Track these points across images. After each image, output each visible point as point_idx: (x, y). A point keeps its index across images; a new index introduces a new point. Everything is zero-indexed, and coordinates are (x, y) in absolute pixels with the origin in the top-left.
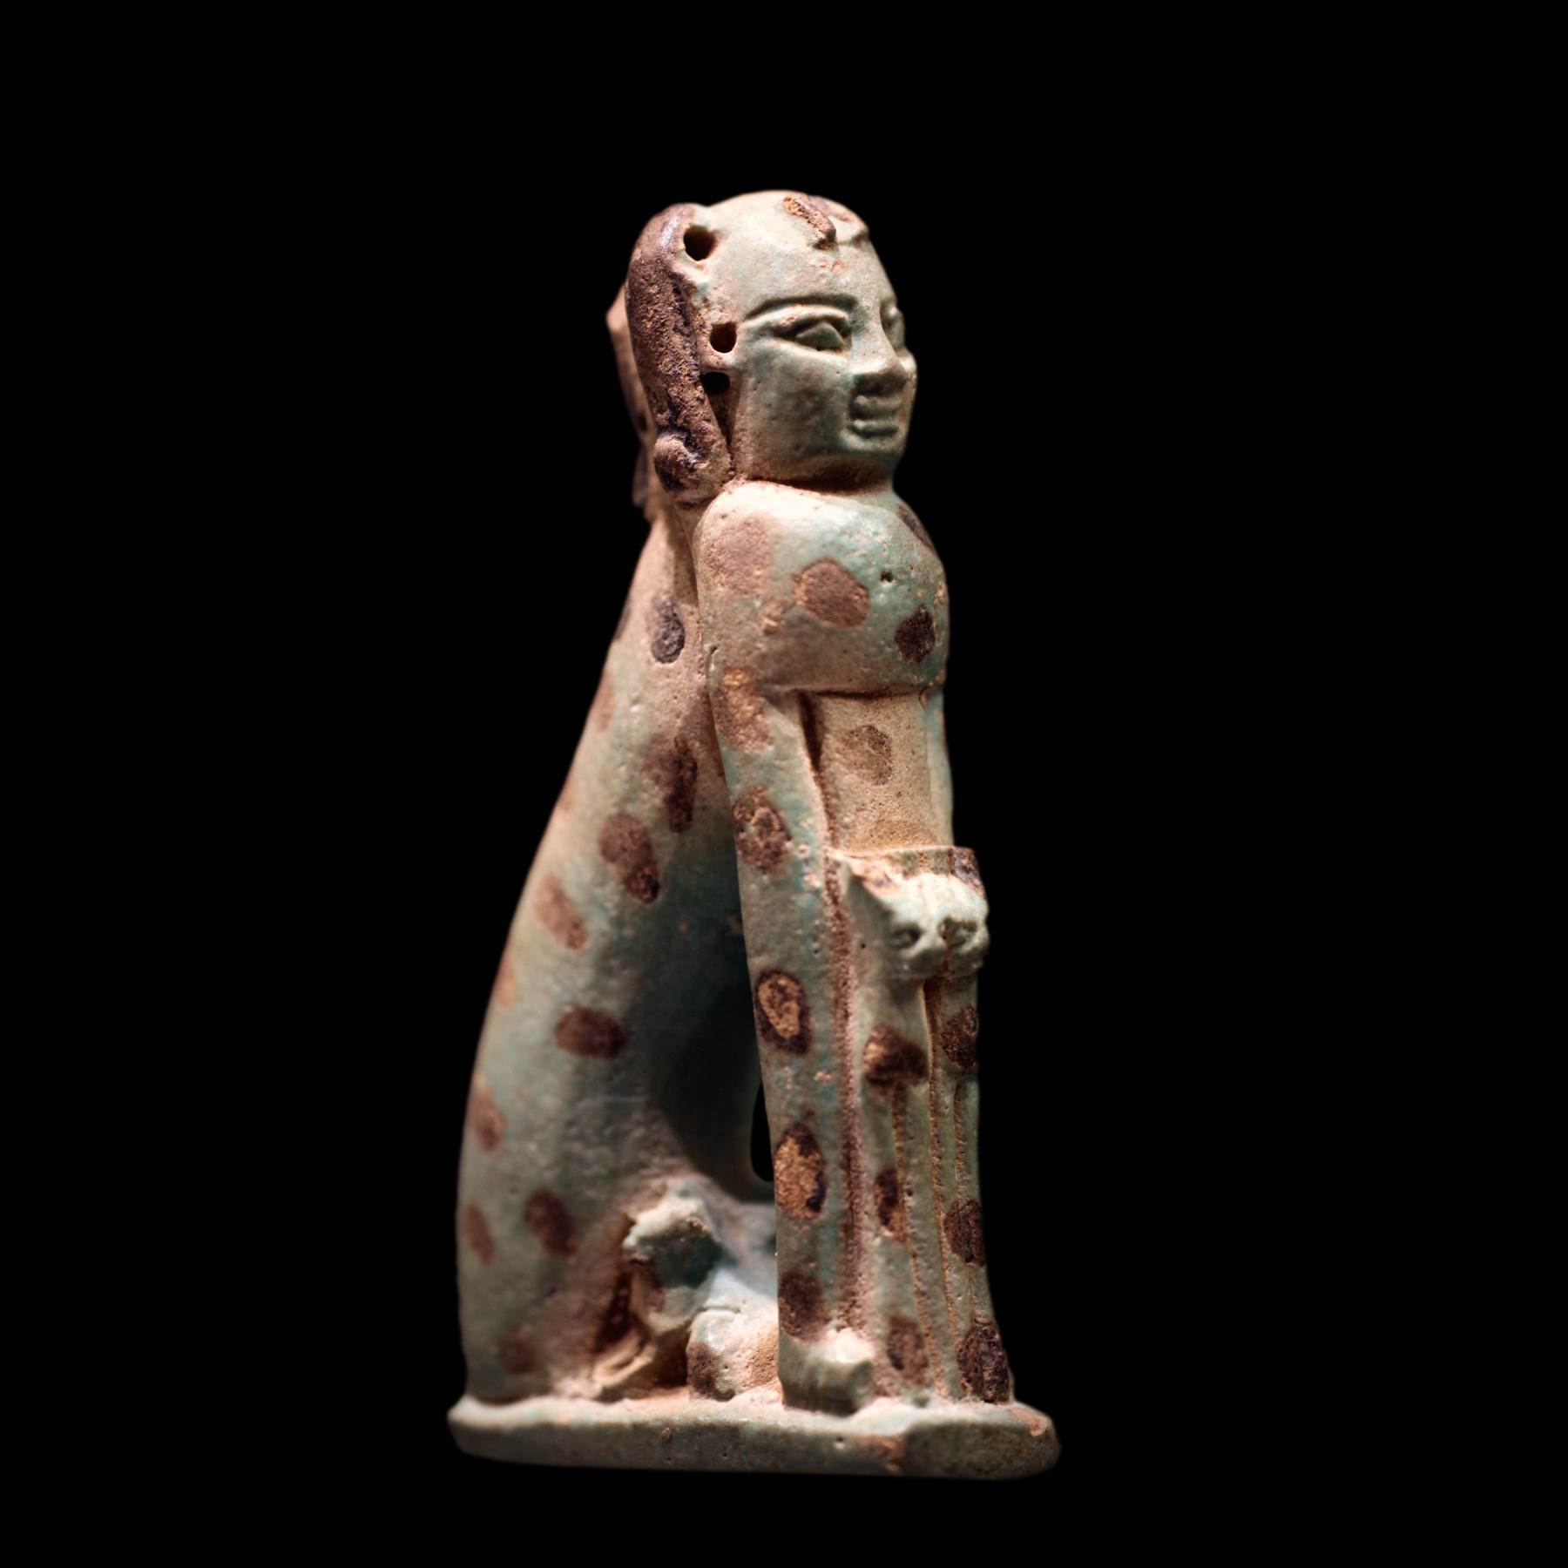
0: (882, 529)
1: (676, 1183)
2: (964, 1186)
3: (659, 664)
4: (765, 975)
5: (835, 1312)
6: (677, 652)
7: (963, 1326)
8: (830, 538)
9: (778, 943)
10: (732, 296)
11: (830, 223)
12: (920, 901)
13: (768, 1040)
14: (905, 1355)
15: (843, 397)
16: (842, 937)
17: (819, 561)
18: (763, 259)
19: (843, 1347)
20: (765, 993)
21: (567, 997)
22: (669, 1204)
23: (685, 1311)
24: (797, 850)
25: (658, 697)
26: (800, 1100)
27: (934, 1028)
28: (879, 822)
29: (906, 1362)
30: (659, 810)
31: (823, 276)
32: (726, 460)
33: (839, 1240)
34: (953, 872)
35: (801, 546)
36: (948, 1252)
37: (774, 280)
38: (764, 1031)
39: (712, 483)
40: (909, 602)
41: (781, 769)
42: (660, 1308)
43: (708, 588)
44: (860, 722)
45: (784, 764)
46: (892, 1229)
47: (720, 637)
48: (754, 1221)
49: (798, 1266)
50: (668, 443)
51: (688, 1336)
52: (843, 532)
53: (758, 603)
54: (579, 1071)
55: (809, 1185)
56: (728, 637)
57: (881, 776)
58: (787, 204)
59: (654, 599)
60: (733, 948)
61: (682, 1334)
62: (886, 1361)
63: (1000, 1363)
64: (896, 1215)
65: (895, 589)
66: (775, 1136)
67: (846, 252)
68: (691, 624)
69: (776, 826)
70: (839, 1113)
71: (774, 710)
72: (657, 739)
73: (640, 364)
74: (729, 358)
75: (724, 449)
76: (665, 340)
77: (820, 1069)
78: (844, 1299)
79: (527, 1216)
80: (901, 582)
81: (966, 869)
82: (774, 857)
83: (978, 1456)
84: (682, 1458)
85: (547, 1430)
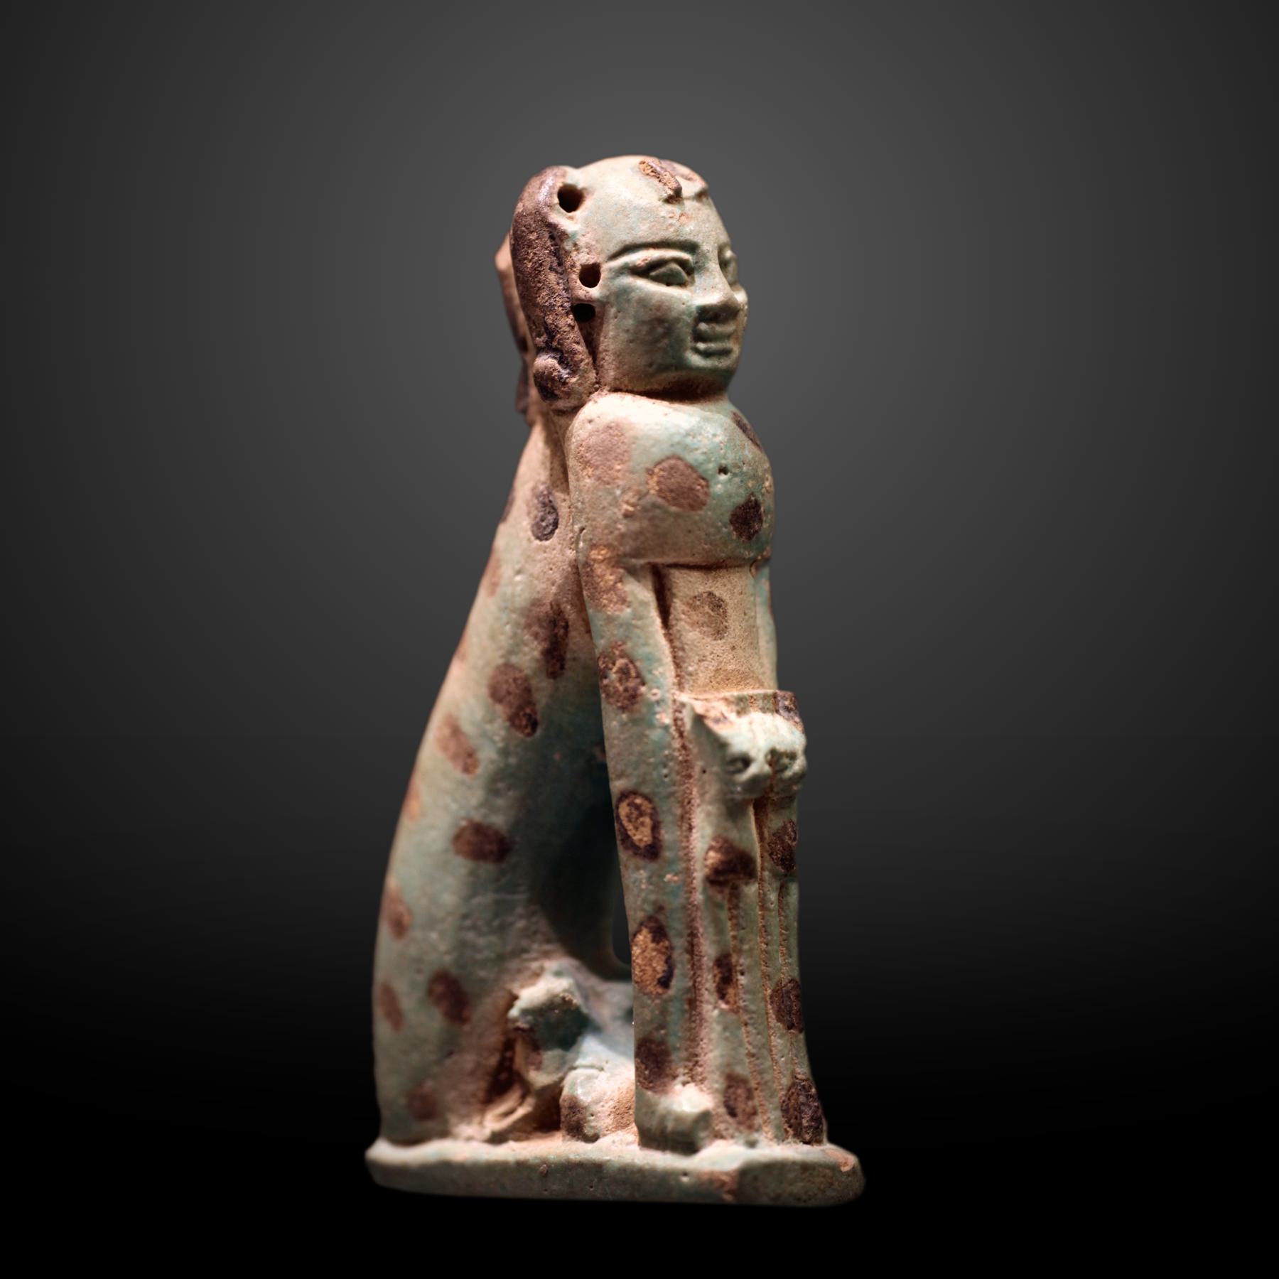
0: (719, 432)
1: (552, 965)
2: (786, 968)
3: (538, 542)
4: (624, 795)
5: (681, 1070)
6: (552, 532)
7: (785, 1081)
8: (677, 439)
9: (635, 769)
10: (597, 241)
11: (677, 182)
12: (751, 735)
13: (626, 848)
14: (738, 1106)
15: (688, 324)
16: (687, 764)
17: (668, 458)
18: (623, 211)
19: (688, 1099)
20: (624, 810)
21: (463, 813)
22: (546, 982)
23: (558, 1069)
24: (650, 693)
25: (536, 569)
26: (652, 897)
27: (762, 839)
28: (717, 670)
29: (739, 1111)
30: (538, 661)
31: (671, 225)
32: (592, 376)
33: (684, 1012)
34: (777, 711)
35: (653, 445)
36: (773, 1021)
37: (632, 228)
38: (623, 841)
39: (581, 394)
40: (742, 491)
41: (637, 627)
42: (539, 1067)
43: (578, 480)
44: (701, 589)
45: (639, 623)
46: (727, 1003)
47: (588, 519)
48: (615, 996)
49: (651, 1032)
50: (545, 362)
51: (561, 1090)
52: (688, 434)
53: (618, 492)
54: (472, 873)
55: (660, 967)
56: (594, 520)
57: (719, 633)
58: (642, 166)
59: (534, 489)
60: (598, 773)
61: (556, 1088)
62: (722, 1110)
63: (815, 1112)
64: (731, 991)
65: (730, 480)
66: (632, 927)
67: (690, 205)
68: (563, 509)
69: (633, 674)
70: (684, 908)
71: (632, 579)
72: (536, 603)
73: (522, 297)
74: (595, 292)
75: (590, 366)
76: (542, 277)
77: (669, 872)
78: (688, 1060)
79: (430, 992)
80: (735, 475)
81: (788, 709)
82: (631, 699)
83: (797, 1188)
84: (556, 1189)
85: (446, 1166)
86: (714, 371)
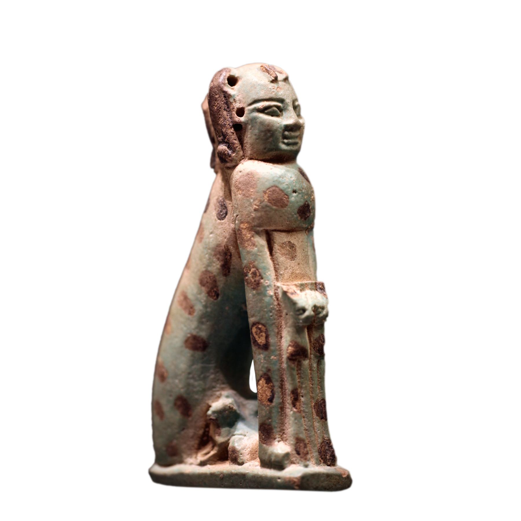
0: (293, 176)
1: (225, 393)
3: (219, 221)
4: (254, 324)
5: (277, 436)
6: (225, 217)
7: (320, 440)
8: (276, 179)
9: (259, 313)
10: (243, 98)
11: (276, 74)
12: (306, 299)
13: (255, 346)
15: (280, 132)
16: (280, 311)
17: (272, 187)
18: (254, 86)
19: (280, 448)
20: (254, 330)
21: (189, 331)
22: (222, 400)
23: (227, 435)
24: (265, 282)
25: (218, 232)
26: (266, 366)
27: (310, 342)
28: (292, 273)
29: (301, 453)
30: (219, 269)
31: (273, 92)
32: (241, 153)
33: (279, 412)
34: (317, 290)
35: (266, 181)
36: (315, 416)
37: (257, 93)
38: (254, 343)
39: (236, 161)
40: (302, 200)
41: (259, 255)
42: (219, 435)
43: (235, 196)
44: (286, 240)
45: (260, 254)
46: (296, 408)
47: (239, 212)
49: (265, 421)
50: (222, 147)
51: (228, 444)
52: (280, 177)
53: (252, 200)
54: (192, 356)
55: (269, 394)
56: (242, 212)
57: (293, 258)
58: (262, 68)
59: (217, 199)
60: (244, 315)
61: (227, 443)
62: (294, 452)
64: (298, 404)
65: (297, 196)
67: (281, 84)
68: (229, 207)
69: (258, 275)
70: (279, 370)
71: (257, 236)
72: (218, 246)
73: (213, 121)
74: (242, 119)
75: (241, 149)
76: (221, 113)
77: (272, 355)
78: (280, 432)
79: (175, 404)
80: (299, 193)
82: (257, 285)
86: (291, 151)
